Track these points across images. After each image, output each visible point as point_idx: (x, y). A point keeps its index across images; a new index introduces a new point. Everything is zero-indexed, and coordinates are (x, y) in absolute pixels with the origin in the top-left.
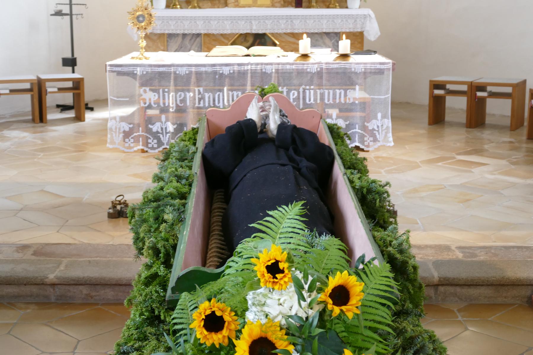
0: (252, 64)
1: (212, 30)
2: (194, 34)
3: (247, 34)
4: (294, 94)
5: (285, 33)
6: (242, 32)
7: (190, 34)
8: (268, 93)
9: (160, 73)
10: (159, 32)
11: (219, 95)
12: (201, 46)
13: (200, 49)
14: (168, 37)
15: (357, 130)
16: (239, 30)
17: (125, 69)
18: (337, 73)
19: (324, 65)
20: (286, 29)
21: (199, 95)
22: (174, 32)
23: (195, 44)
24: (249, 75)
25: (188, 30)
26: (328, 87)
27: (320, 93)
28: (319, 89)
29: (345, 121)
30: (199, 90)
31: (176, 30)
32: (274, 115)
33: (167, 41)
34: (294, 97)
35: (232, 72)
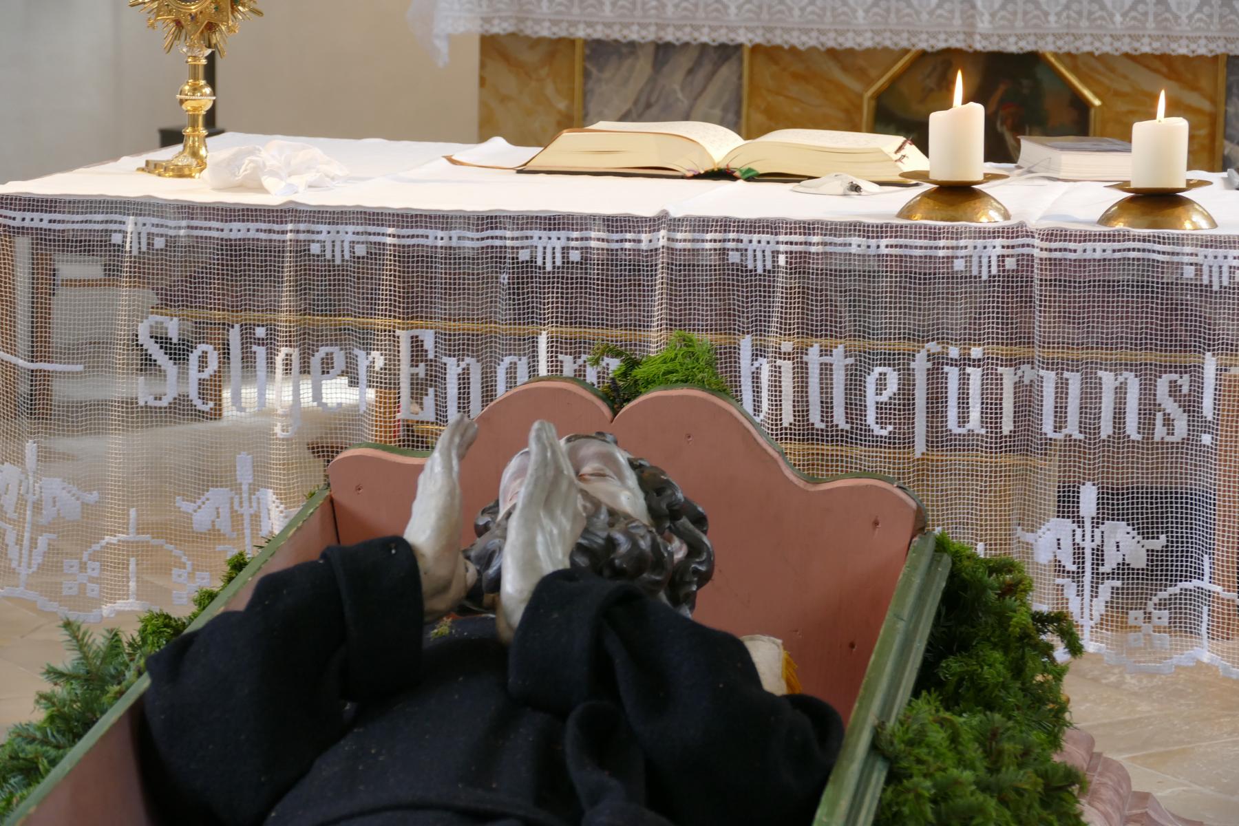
0: (675, 224)
1: (787, 31)
2: (704, 46)
3: (948, 51)
4: (881, 384)
5: (1127, 55)
6: (923, 45)
7: (687, 44)
8: (649, 383)
9: (234, 251)
10: (545, 32)
11: (513, 366)
12: (740, 102)
13: (731, 117)
14: (586, 58)
15: (1205, 584)
16: (913, 34)
17: (71, 223)
18: (1110, 286)
19: (1037, 242)
20: (1137, 38)
21: (414, 362)
22: (616, 34)
23: (712, 89)
24: (661, 276)
25: (679, 28)
26: (1057, 354)
27: (1017, 385)
28: (1014, 362)
29: (1147, 532)
30: (416, 344)
31: (627, 26)
32: (530, 524)
33: (586, 75)
34: (884, 398)
35: (575, 256)
